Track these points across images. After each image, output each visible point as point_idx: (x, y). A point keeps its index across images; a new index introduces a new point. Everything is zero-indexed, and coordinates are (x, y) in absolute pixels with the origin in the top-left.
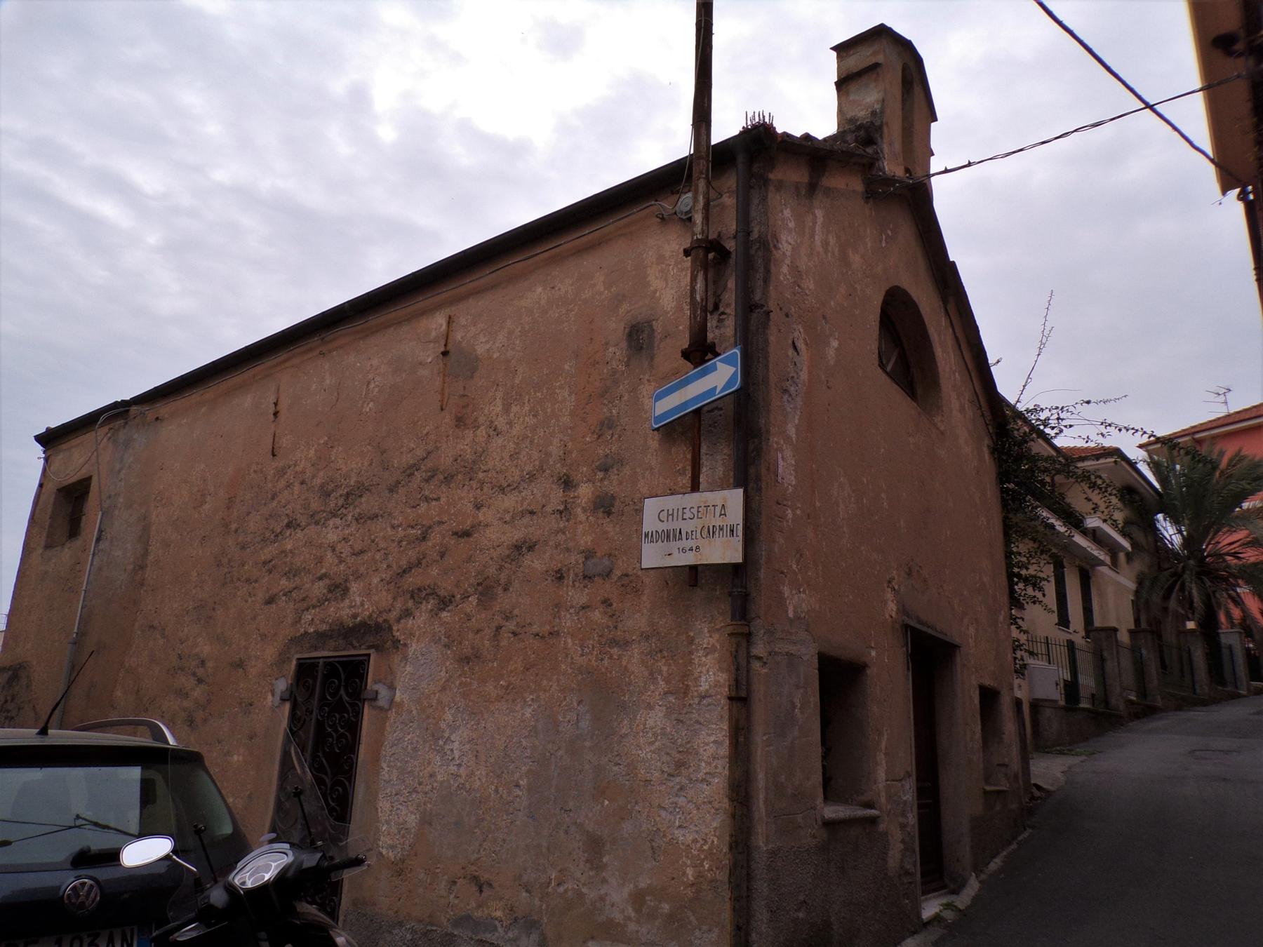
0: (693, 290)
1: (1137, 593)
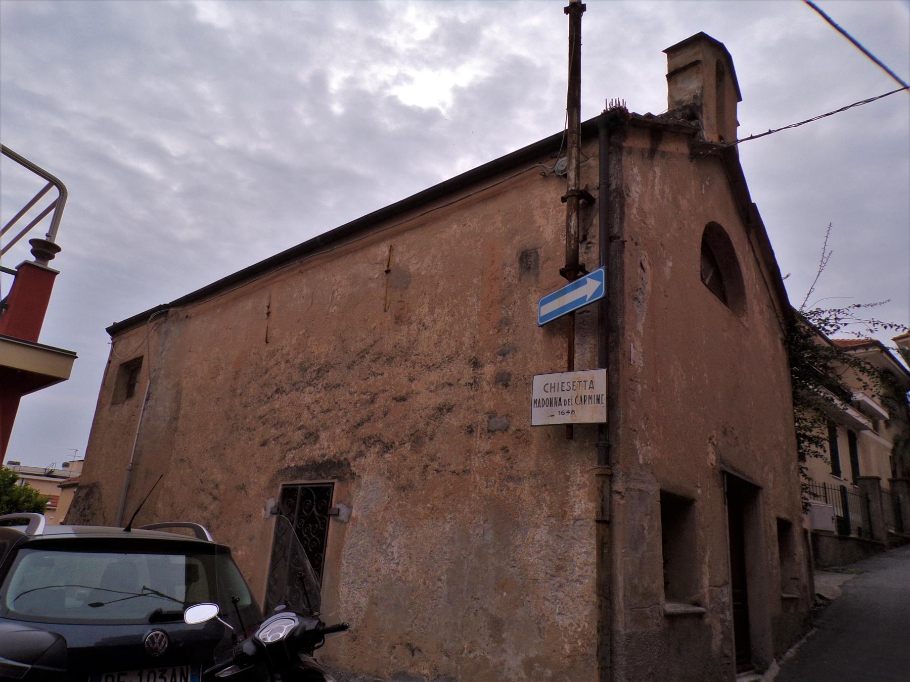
0: (568, 226)
1: (893, 451)
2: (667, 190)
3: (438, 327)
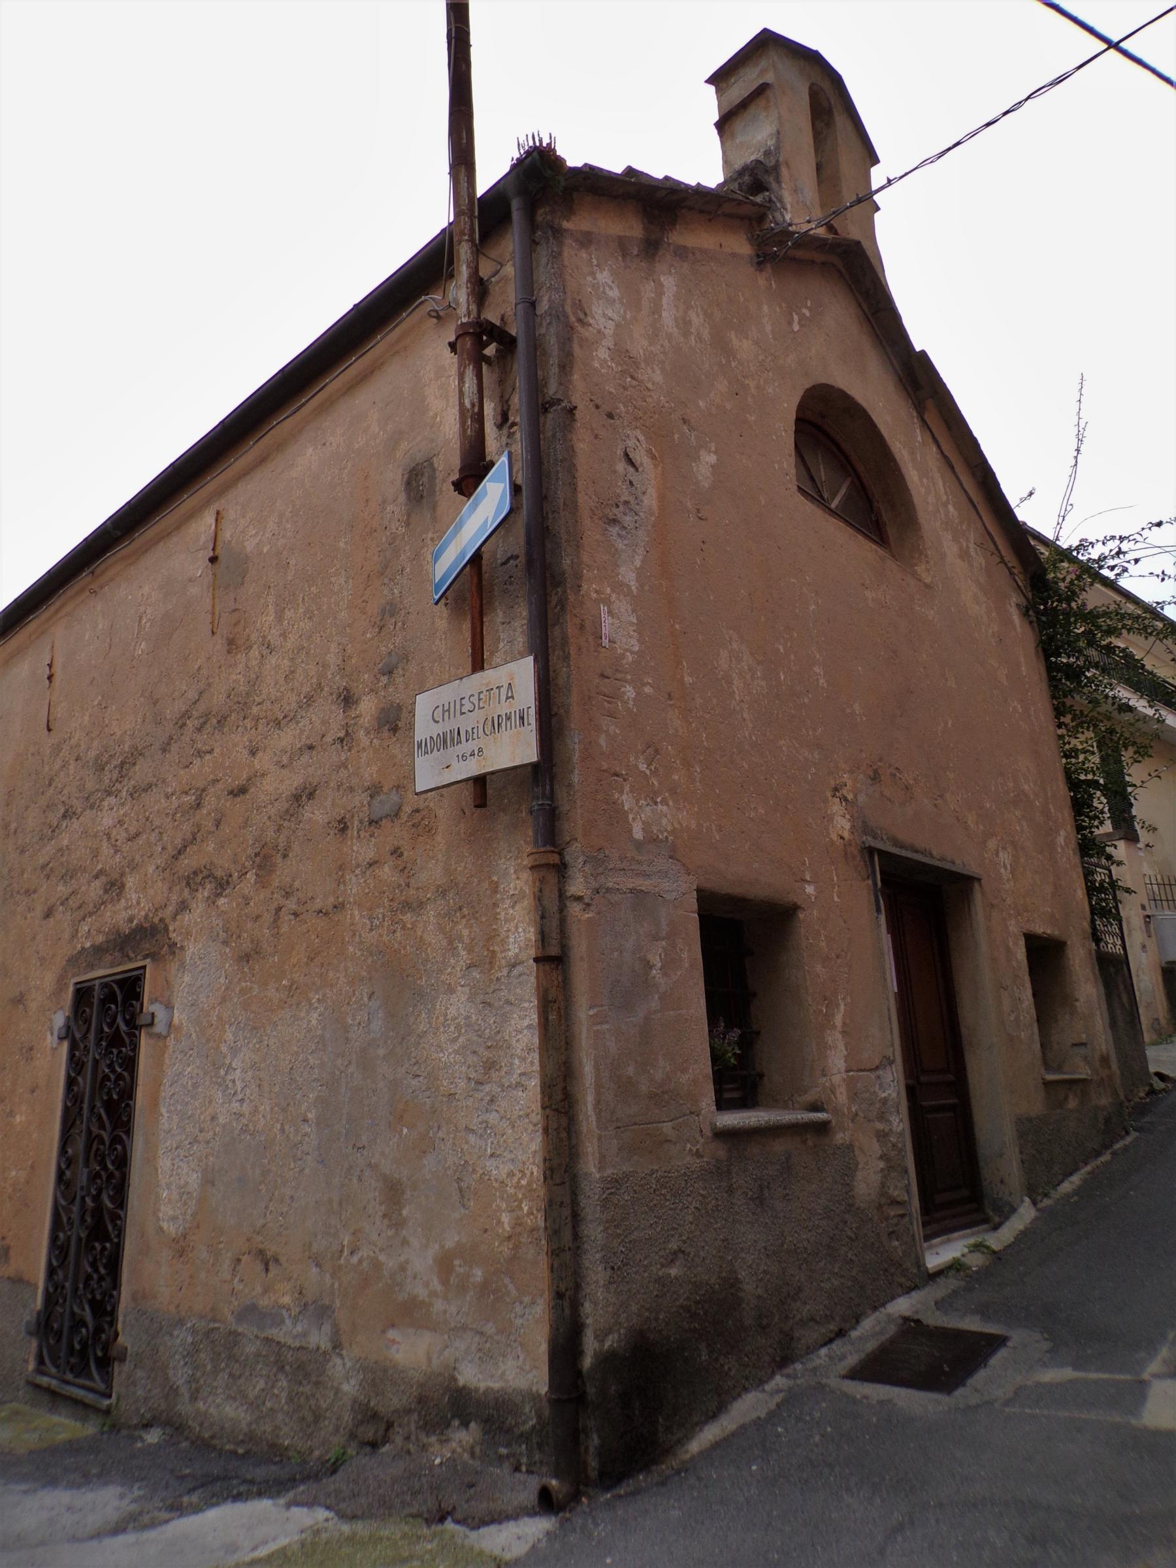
2: (696, 319)
3: (289, 645)
